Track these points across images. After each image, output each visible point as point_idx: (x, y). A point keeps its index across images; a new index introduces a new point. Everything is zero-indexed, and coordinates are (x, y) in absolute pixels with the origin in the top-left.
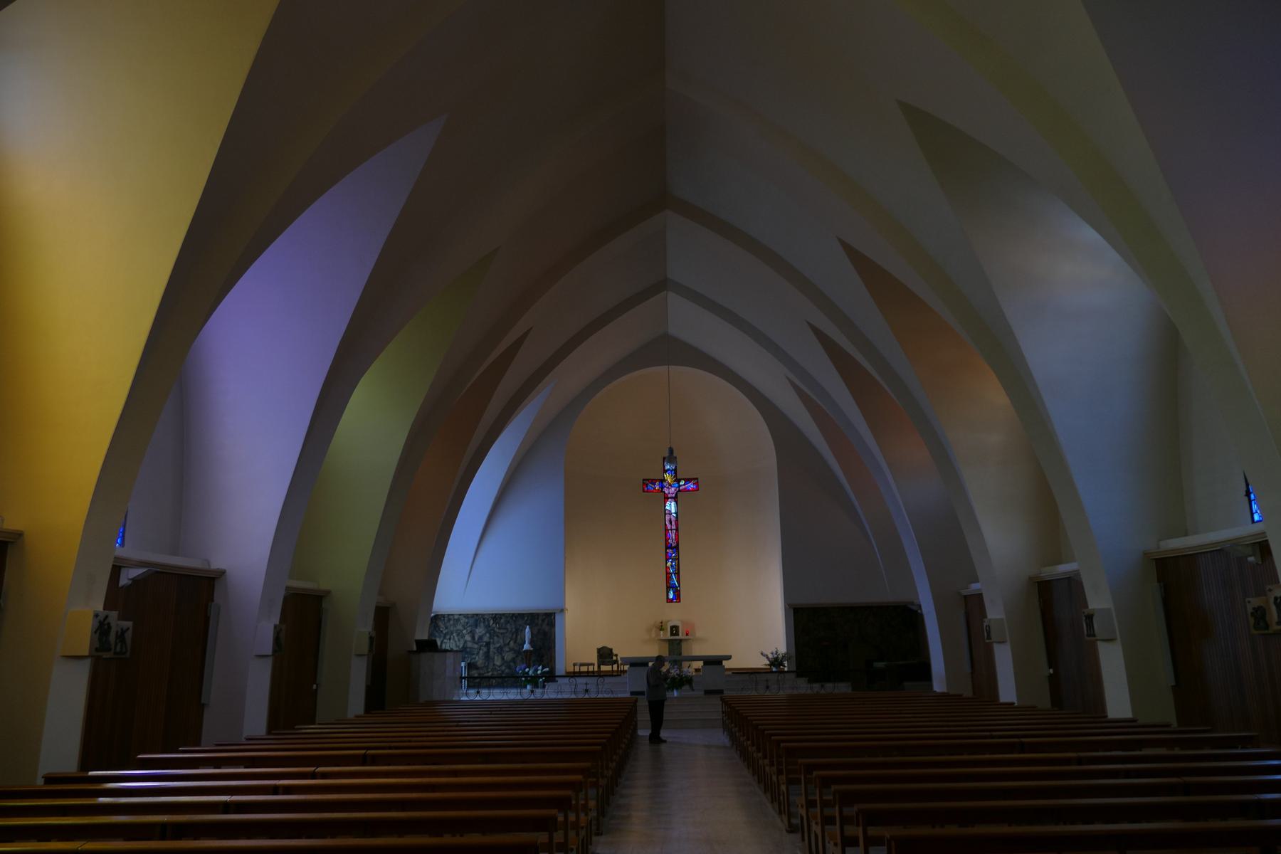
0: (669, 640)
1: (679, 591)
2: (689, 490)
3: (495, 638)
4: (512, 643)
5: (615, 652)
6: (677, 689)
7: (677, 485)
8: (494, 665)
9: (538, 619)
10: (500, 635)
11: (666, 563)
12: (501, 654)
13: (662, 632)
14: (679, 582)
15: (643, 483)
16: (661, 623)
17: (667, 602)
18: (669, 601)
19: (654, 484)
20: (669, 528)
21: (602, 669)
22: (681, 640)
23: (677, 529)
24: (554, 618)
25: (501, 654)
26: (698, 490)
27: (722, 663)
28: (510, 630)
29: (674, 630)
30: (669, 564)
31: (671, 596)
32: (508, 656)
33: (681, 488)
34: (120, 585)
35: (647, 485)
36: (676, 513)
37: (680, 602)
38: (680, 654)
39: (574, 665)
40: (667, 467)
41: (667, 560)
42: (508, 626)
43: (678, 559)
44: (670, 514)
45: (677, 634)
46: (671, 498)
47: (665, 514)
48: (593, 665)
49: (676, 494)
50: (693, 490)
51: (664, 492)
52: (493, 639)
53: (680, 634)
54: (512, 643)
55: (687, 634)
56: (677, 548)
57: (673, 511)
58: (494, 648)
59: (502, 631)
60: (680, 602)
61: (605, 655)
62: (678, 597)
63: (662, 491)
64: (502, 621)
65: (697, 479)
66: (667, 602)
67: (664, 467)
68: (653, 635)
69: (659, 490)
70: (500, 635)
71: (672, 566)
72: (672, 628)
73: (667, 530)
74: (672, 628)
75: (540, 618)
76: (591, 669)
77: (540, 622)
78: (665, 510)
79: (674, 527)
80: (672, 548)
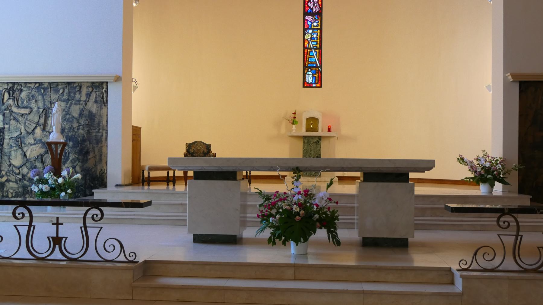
0: (304, 137)
1: (321, 72)
3: (12, 122)
4: (38, 131)
5: (213, 150)
6: (297, 242)
8: (10, 165)
9: (80, 91)
10: (20, 118)
11: (304, 34)
12: (21, 148)
13: (294, 126)
14: (320, 60)
16: (294, 113)
17: (304, 86)
18: (306, 85)
21: (243, 172)
22: (320, 138)
24: (107, 92)
25: (21, 148)
28: (35, 109)
29: (312, 123)
30: (308, 36)
31: (310, 79)
32: (34, 151)
37: (321, 87)
38: (319, 156)
42: (33, 105)
43: (321, 29)
45: (316, 130)
52: (9, 123)
53: (320, 130)
54: (38, 131)
55: (329, 130)
56: (320, 14)
58: (11, 138)
59: (23, 111)
60: (321, 87)
62: (319, 81)
64: (24, 94)
66: (304, 86)
68: (283, 131)
70: (20, 118)
71: (312, 38)
72: (308, 120)
74: (308, 120)
75: (84, 91)
77: (84, 98)
80: (312, 14)
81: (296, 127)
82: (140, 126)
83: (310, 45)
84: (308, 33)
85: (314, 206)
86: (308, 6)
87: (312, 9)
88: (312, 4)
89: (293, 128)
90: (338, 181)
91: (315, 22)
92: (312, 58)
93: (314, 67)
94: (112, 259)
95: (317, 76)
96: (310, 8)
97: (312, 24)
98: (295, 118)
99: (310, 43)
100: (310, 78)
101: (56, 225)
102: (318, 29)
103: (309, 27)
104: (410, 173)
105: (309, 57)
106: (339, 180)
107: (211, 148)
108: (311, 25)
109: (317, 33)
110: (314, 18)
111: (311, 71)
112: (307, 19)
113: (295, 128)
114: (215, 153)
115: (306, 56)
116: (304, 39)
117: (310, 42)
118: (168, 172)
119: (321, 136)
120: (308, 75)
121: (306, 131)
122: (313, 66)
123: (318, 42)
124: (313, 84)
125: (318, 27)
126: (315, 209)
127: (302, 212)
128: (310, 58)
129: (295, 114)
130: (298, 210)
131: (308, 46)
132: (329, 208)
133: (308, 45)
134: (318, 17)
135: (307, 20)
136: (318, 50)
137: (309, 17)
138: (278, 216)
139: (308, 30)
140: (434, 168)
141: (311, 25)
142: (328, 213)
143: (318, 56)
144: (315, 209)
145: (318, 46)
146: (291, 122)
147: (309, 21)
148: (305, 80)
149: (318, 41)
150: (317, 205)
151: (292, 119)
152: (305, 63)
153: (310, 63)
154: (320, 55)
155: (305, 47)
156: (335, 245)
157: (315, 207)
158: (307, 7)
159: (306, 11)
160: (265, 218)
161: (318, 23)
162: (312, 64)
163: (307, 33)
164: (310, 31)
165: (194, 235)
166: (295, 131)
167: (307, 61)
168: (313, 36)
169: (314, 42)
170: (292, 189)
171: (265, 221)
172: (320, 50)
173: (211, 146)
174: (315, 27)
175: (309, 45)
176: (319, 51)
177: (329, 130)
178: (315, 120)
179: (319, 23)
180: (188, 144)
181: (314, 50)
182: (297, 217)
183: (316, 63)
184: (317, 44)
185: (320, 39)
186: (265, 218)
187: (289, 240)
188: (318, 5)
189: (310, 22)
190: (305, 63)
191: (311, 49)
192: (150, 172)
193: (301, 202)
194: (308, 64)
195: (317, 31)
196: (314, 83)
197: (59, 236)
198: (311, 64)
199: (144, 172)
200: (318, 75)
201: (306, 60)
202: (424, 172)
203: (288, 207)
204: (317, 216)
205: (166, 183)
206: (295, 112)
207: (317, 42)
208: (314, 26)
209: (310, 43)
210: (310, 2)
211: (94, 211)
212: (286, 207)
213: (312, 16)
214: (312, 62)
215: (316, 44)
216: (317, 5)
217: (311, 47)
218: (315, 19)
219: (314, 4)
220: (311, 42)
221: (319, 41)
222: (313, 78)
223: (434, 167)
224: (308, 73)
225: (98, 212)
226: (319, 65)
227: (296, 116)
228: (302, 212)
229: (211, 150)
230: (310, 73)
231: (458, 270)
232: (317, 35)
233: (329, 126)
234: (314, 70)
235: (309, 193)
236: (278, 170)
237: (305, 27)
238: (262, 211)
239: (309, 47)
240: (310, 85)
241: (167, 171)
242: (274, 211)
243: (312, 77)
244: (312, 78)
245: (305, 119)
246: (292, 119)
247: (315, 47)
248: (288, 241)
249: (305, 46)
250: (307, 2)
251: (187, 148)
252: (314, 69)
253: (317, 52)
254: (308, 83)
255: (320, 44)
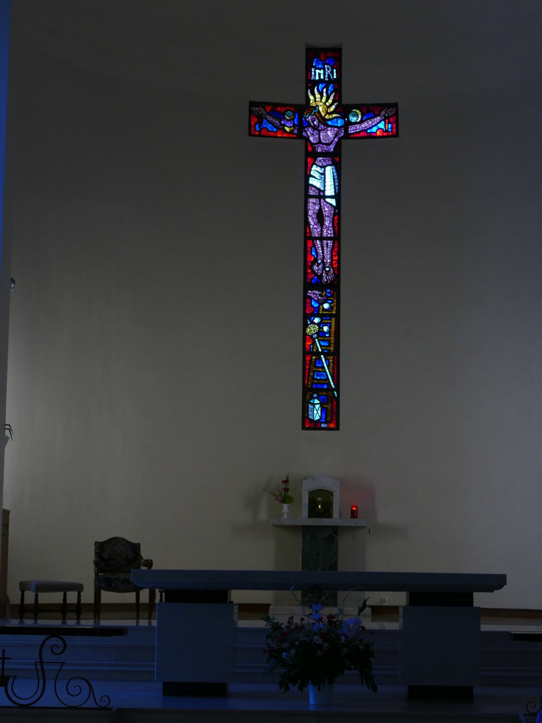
0: (305, 528)
2: (372, 136)
5: (145, 554)
7: (340, 123)
11: (306, 326)
13: (285, 507)
15: (251, 112)
16: (286, 481)
17: (304, 428)
19: (280, 116)
20: (316, 234)
22: (335, 530)
23: (336, 238)
26: (396, 135)
27: (470, 601)
30: (312, 330)
31: (316, 414)
33: (351, 130)
34: (101, 590)
35: (260, 119)
36: (337, 196)
37: (337, 428)
38: (334, 566)
39: (24, 587)
40: (318, 74)
41: (307, 318)
43: (337, 316)
44: (321, 195)
45: (327, 512)
46: (324, 154)
47: (307, 196)
48: (78, 588)
49: (338, 145)
50: (386, 135)
51: (307, 139)
55: (354, 515)
57: (330, 191)
60: (337, 428)
61: (322, 610)
63: (300, 136)
65: (395, 105)
66: (304, 428)
67: (308, 72)
68: (263, 515)
69: (291, 132)
71: (320, 333)
73: (308, 238)
74: (313, 495)
76: (72, 597)
78: (307, 186)
79: (328, 232)
80: (318, 285)
81: (289, 508)
82: (8, 509)
83: (317, 346)
84: (312, 322)
85: (342, 636)
86: (313, 271)
87: (321, 276)
88: (320, 266)
89: (283, 511)
90: (370, 613)
91: (326, 302)
92: (319, 371)
93: (324, 390)
94: (77, 705)
95: (328, 407)
96: (316, 274)
97: (321, 306)
98: (286, 490)
99: (317, 342)
100: (315, 412)
101: (5, 657)
102: (331, 316)
103: (315, 312)
104: (476, 595)
105: (314, 369)
106: (372, 613)
107: (140, 551)
108: (319, 307)
109: (330, 324)
110: (324, 294)
111: (317, 398)
112: (310, 296)
113: (288, 511)
114: (151, 561)
115: (307, 367)
116: (305, 334)
117: (316, 340)
118: (65, 595)
119: (337, 527)
120: (313, 406)
121: (310, 516)
122: (321, 388)
123: (333, 342)
124: (323, 423)
125: (332, 311)
126: (343, 641)
127: (326, 645)
128: (315, 373)
129: (287, 483)
130: (320, 641)
131: (313, 348)
132: (361, 640)
133: (312, 346)
134: (332, 293)
135: (311, 298)
136: (332, 357)
137: (314, 291)
138: (293, 651)
139: (312, 318)
140: (505, 586)
141: (319, 307)
142: (362, 647)
143: (331, 368)
144: (343, 641)
145: (332, 349)
146: (280, 498)
147: (315, 301)
148: (306, 415)
149: (332, 338)
150: (346, 636)
151: (281, 494)
152: (306, 382)
153: (315, 381)
154: (335, 367)
155: (307, 350)
156: (370, 690)
157: (343, 638)
158: (310, 273)
159: (309, 281)
160: (274, 654)
161: (332, 305)
162: (321, 383)
163: (310, 324)
164: (317, 320)
165: (165, 684)
166: (288, 516)
167: (310, 378)
168: (321, 330)
169: (323, 341)
170: (310, 615)
171: (273, 660)
172: (336, 358)
173: (140, 547)
174: (327, 313)
175: (315, 347)
176: (333, 359)
177: (354, 515)
178: (327, 494)
179: (335, 303)
180: (98, 542)
181: (324, 357)
182: (320, 653)
183: (328, 382)
184: (329, 346)
185: (335, 336)
186: (274, 654)
187: (307, 684)
188: (332, 270)
189: (316, 301)
190: (306, 382)
191: (318, 354)
192: (39, 594)
193: (323, 631)
194: (312, 384)
195: (331, 320)
196: (324, 421)
197: (5, 675)
198: (319, 383)
199: (25, 593)
200: (332, 406)
201: (309, 376)
202: (493, 591)
203: (306, 639)
204: (345, 650)
205: (60, 615)
206: (288, 478)
207: (329, 341)
208: (324, 309)
209: (317, 342)
210: (316, 264)
211: (53, 641)
212: (303, 639)
213: (319, 291)
214: (321, 379)
215: (327, 344)
216: (330, 270)
217: (318, 349)
218: (326, 295)
219: (324, 268)
220: (319, 341)
221: (334, 340)
222: (321, 410)
223: (506, 585)
224: (312, 401)
225: (60, 643)
226: (333, 386)
227: (290, 486)
228: (326, 645)
229: (140, 554)
230: (317, 401)
231: (525, 715)
232: (330, 328)
233: (352, 507)
234: (324, 395)
235: (334, 620)
236: (292, 588)
237: (307, 312)
238: (270, 644)
239: (315, 350)
240: (315, 425)
241: (63, 593)
242: (285, 645)
243: (320, 409)
244: (319, 412)
245: (307, 493)
246: (281, 491)
247: (325, 351)
248: (306, 687)
249: (307, 348)
250: (310, 264)
251: (98, 550)
252: (325, 393)
253: (329, 360)
254: (312, 421)
255: (335, 344)
